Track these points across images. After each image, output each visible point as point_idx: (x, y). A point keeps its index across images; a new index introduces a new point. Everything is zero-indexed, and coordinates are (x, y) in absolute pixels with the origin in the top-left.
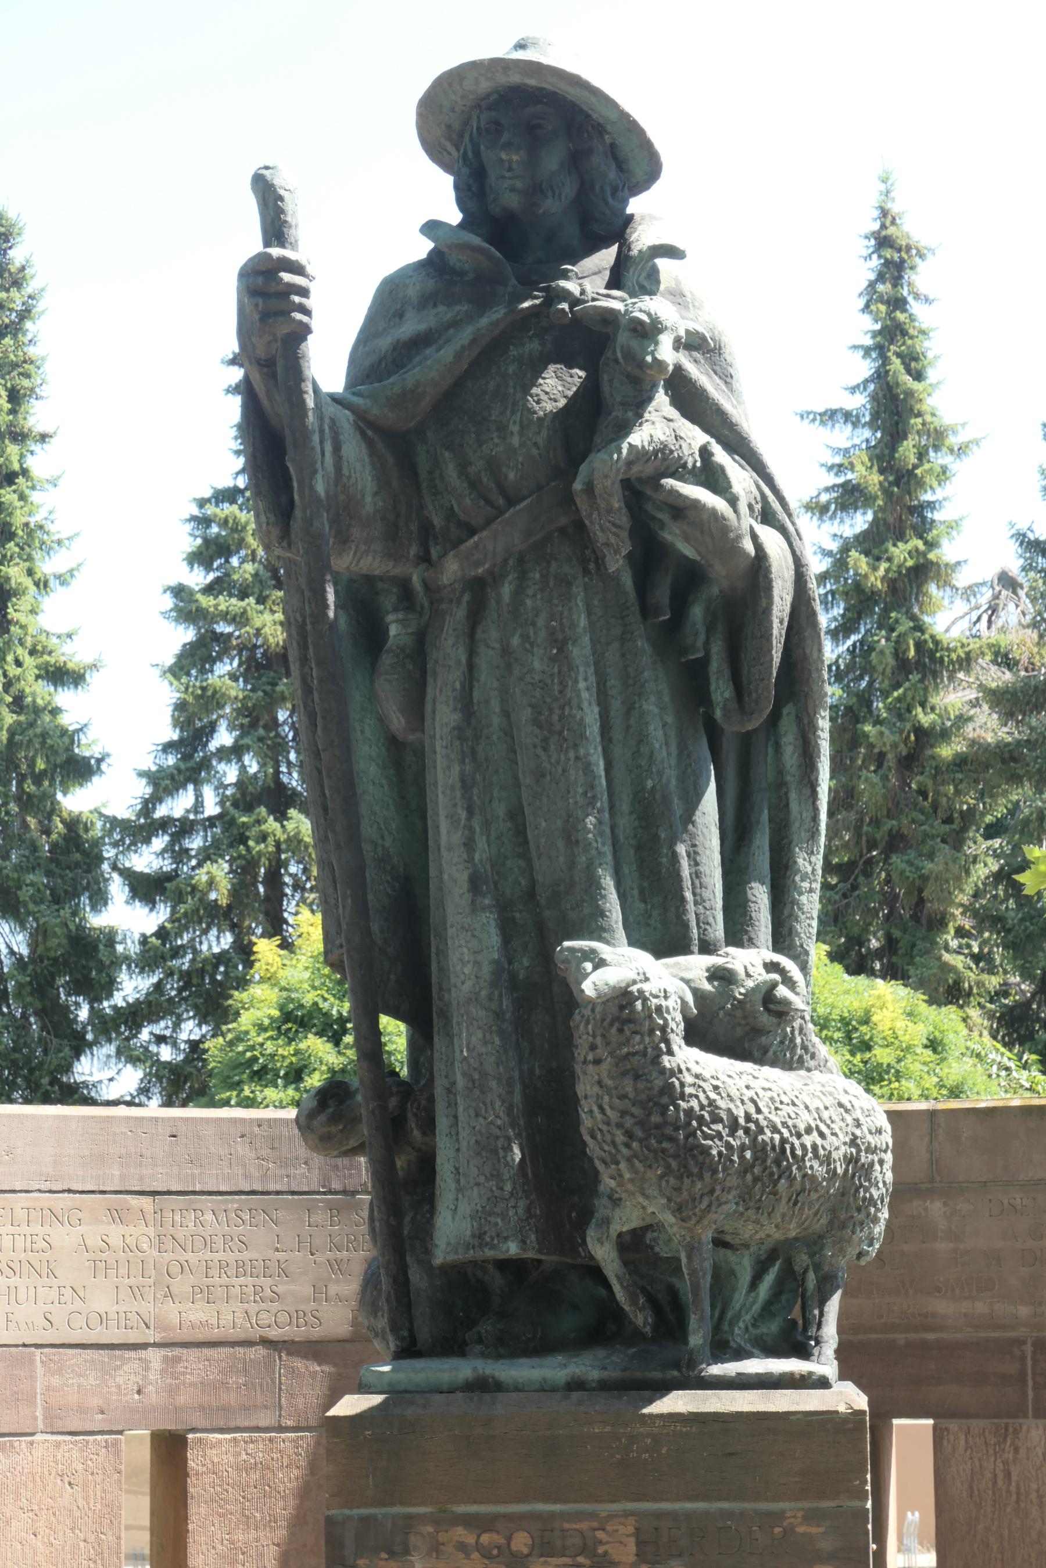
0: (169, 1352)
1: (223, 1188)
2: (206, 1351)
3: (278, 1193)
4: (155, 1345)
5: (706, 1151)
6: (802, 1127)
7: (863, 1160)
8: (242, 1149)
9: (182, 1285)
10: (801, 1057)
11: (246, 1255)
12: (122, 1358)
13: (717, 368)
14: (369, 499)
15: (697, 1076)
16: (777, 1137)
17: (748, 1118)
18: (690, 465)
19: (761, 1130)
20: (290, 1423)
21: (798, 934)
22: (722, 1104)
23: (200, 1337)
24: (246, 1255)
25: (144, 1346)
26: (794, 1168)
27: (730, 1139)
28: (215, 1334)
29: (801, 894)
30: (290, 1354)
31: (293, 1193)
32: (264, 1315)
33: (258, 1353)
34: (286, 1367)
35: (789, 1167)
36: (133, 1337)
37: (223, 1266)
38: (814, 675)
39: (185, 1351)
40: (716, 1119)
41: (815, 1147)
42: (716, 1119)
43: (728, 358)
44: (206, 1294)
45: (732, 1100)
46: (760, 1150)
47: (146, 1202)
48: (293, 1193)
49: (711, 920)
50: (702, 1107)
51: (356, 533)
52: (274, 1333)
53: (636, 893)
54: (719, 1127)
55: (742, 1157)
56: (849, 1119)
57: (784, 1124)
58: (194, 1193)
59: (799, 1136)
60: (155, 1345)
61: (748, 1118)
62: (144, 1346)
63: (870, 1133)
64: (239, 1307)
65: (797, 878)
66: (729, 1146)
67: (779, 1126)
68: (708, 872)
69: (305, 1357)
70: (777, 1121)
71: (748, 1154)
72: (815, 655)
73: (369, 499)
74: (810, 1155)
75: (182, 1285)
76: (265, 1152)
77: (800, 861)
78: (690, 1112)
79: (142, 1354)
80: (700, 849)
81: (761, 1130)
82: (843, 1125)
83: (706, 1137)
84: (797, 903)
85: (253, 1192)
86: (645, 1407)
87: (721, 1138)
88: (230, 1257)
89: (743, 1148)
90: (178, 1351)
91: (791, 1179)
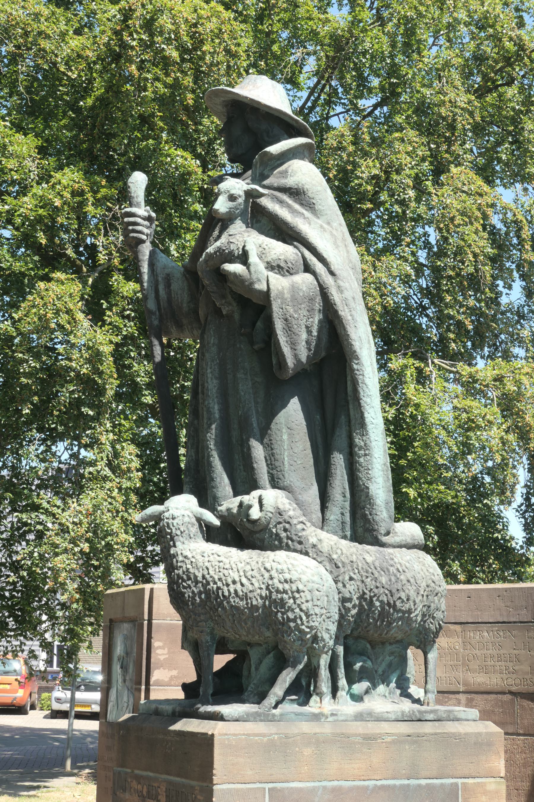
0: (469, 696)
1: (491, 621)
2: (485, 696)
3: (515, 622)
4: (463, 692)
5: (183, 594)
6: (230, 581)
7: (274, 597)
8: (499, 602)
9: (474, 665)
10: (287, 544)
11: (502, 652)
12: (448, 698)
13: (304, 202)
14: (185, 305)
15: (186, 557)
16: (215, 586)
17: (204, 577)
18: (236, 255)
19: (208, 583)
20: (521, 732)
21: (361, 479)
22: (192, 570)
23: (482, 689)
24: (502, 652)
25: (458, 693)
26: (225, 602)
27: (194, 589)
28: (489, 688)
29: (359, 457)
30: (521, 698)
31: (521, 622)
32: (510, 680)
33: (507, 698)
34: (520, 705)
35: (222, 602)
36: (453, 688)
37: (492, 657)
38: (345, 343)
39: (476, 695)
40: (189, 578)
41: (236, 591)
42: (189, 578)
43: (310, 195)
44: (484, 669)
45: (198, 569)
46: (207, 592)
47: (458, 628)
48: (521, 622)
49: (281, 476)
50: (184, 572)
51: (185, 321)
52: (514, 689)
53: (242, 467)
54: (189, 582)
55: (200, 597)
56: (267, 575)
57: (220, 579)
58: (479, 623)
59: (228, 585)
60: (463, 692)
61: (204, 577)
62: (458, 693)
63: (280, 582)
64: (499, 676)
65: (356, 449)
66: (193, 592)
67: (217, 580)
68: (279, 452)
69: (528, 699)
70: (216, 577)
71: (203, 596)
72: (343, 332)
73: (185, 305)
74: (233, 595)
75: (474, 665)
76: (509, 604)
77: (357, 440)
78: (178, 575)
79: (457, 696)
80: (274, 442)
81: (208, 583)
82: (261, 578)
83: (184, 587)
84: (358, 462)
85: (504, 622)
86: (171, 725)
87: (190, 588)
88: (495, 652)
89: (200, 593)
90: (473, 695)
91: (224, 608)
